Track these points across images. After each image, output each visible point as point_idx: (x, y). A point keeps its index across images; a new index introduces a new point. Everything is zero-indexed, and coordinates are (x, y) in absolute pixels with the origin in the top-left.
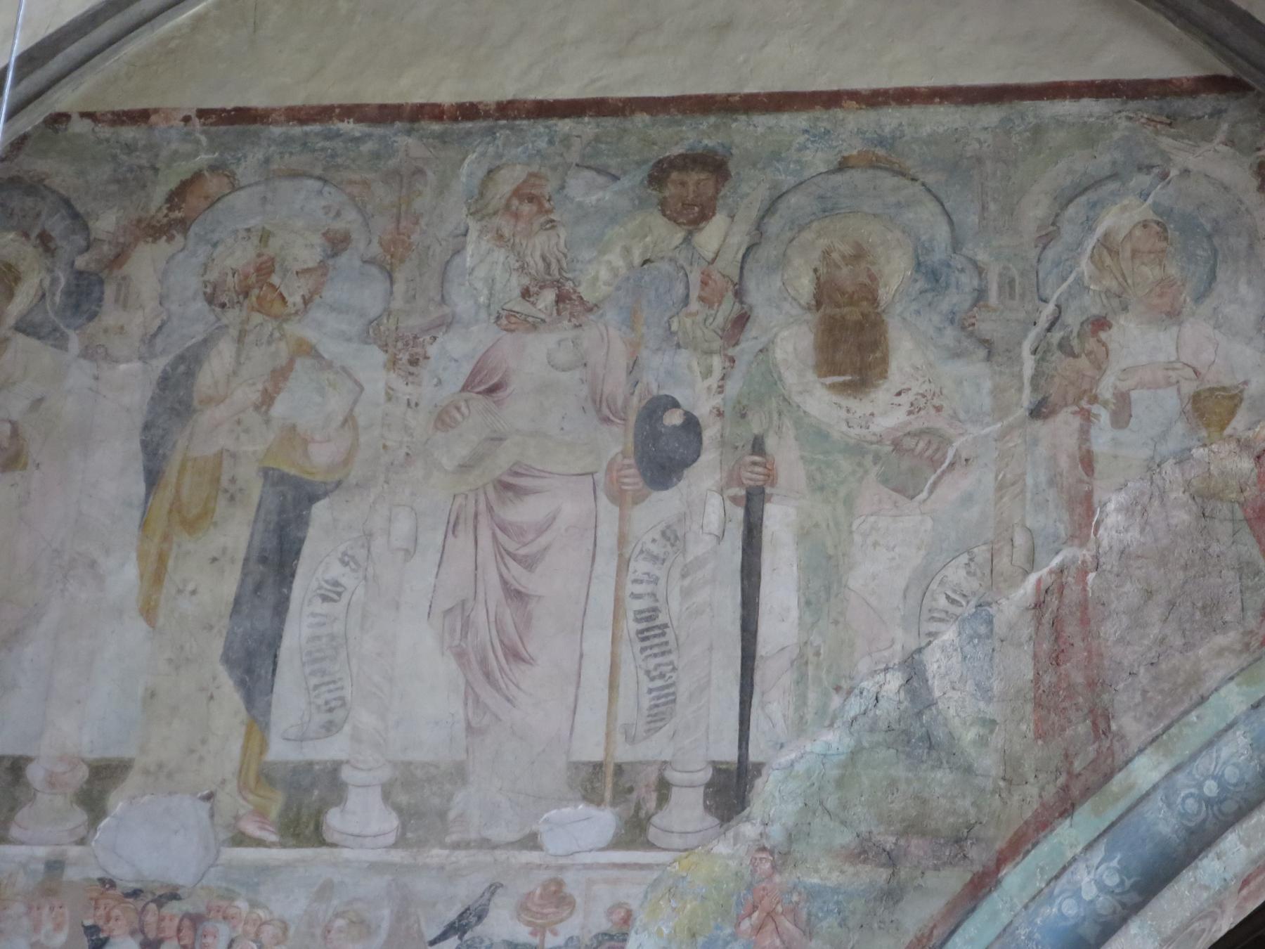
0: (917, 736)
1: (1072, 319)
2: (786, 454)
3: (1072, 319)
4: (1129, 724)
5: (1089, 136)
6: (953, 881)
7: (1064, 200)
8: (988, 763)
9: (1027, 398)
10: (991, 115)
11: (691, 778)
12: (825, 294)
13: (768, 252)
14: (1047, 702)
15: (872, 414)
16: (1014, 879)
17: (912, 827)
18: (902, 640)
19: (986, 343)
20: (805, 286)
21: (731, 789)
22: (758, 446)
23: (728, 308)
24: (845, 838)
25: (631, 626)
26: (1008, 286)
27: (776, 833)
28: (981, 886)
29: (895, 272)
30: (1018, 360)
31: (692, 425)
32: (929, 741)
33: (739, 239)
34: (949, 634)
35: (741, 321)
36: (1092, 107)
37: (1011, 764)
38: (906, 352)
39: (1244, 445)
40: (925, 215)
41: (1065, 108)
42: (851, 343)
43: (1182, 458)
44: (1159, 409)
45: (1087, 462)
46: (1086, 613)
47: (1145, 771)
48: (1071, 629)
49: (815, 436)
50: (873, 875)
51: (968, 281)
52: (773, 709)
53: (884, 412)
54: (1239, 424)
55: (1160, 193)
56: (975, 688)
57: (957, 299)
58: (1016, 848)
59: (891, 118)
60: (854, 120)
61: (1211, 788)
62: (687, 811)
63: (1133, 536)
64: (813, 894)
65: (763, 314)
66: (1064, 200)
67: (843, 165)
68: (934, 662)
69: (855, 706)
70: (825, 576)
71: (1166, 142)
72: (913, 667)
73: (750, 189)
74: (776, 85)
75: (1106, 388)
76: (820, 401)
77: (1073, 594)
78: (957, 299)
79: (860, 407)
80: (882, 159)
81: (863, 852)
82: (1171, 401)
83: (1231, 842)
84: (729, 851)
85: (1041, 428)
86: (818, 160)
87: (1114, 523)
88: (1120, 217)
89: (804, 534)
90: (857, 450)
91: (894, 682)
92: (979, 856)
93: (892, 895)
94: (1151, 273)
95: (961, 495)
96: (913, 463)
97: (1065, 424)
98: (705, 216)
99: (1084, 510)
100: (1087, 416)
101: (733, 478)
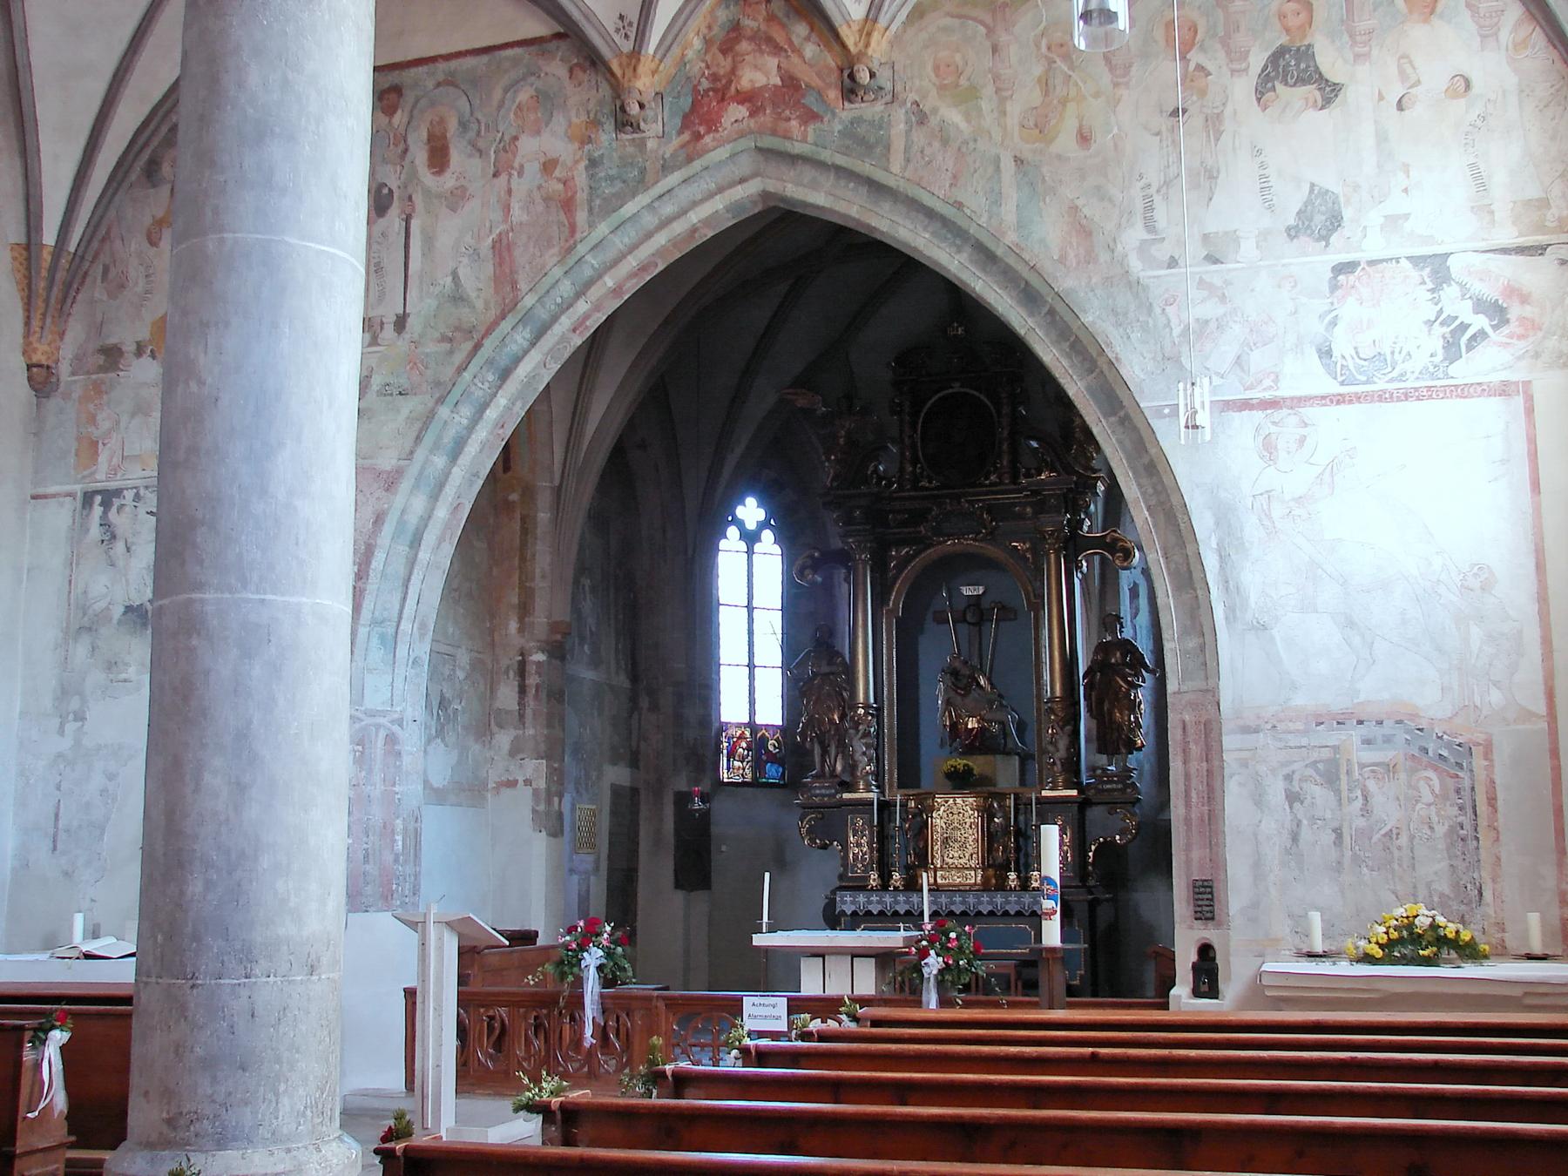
0: (457, 297)
1: (507, 138)
2: (418, 199)
3: (507, 138)
4: (523, 286)
5: (516, 62)
6: (469, 346)
7: (506, 91)
8: (479, 304)
9: (492, 170)
10: (485, 59)
11: (390, 319)
12: (431, 138)
13: (414, 123)
14: (497, 280)
15: (111, 777)
16: (489, 344)
17: (457, 329)
18: (451, 265)
19: (480, 151)
20: (425, 135)
21: (401, 323)
22: (410, 198)
23: (402, 146)
24: (437, 335)
25: (373, 268)
26: (487, 126)
27: (416, 337)
28: (477, 347)
29: (453, 126)
30: (488, 155)
31: (391, 191)
32: (462, 299)
33: (405, 120)
34: (465, 260)
35: (406, 151)
36: (518, 51)
37: (487, 303)
38: (456, 157)
39: (559, 180)
40: (463, 103)
41: (509, 52)
42: (439, 157)
43: (539, 187)
44: (532, 169)
45: (509, 192)
46: (509, 247)
47: (529, 301)
48: (505, 254)
49: (427, 193)
50: (446, 346)
51: (475, 126)
52: (413, 293)
53: (449, 181)
54: (557, 173)
55: (539, 84)
56: (476, 280)
57: (471, 134)
58: (489, 332)
59: (454, 64)
60: (442, 66)
61: (559, 300)
62: (389, 332)
63: (525, 218)
64: (427, 355)
65: (412, 148)
66: (506, 91)
67: (439, 85)
68: (461, 272)
69: (437, 290)
70: (429, 241)
71: (541, 62)
72: (455, 275)
73: (409, 97)
74: (416, 56)
75: (516, 165)
76: (427, 177)
77: (505, 242)
78: (471, 134)
79: (441, 179)
80: (450, 81)
81: (444, 339)
82: (536, 166)
83: (563, 319)
84: (402, 344)
85: (496, 181)
86: (430, 84)
87: (517, 214)
88: (524, 96)
89: (423, 231)
90: (439, 196)
91: (450, 279)
92: (476, 336)
93: (451, 352)
94: (532, 117)
95: (472, 208)
96: (456, 198)
97: (503, 177)
98: (395, 112)
99: (507, 209)
100: (510, 175)
101: (403, 212)
